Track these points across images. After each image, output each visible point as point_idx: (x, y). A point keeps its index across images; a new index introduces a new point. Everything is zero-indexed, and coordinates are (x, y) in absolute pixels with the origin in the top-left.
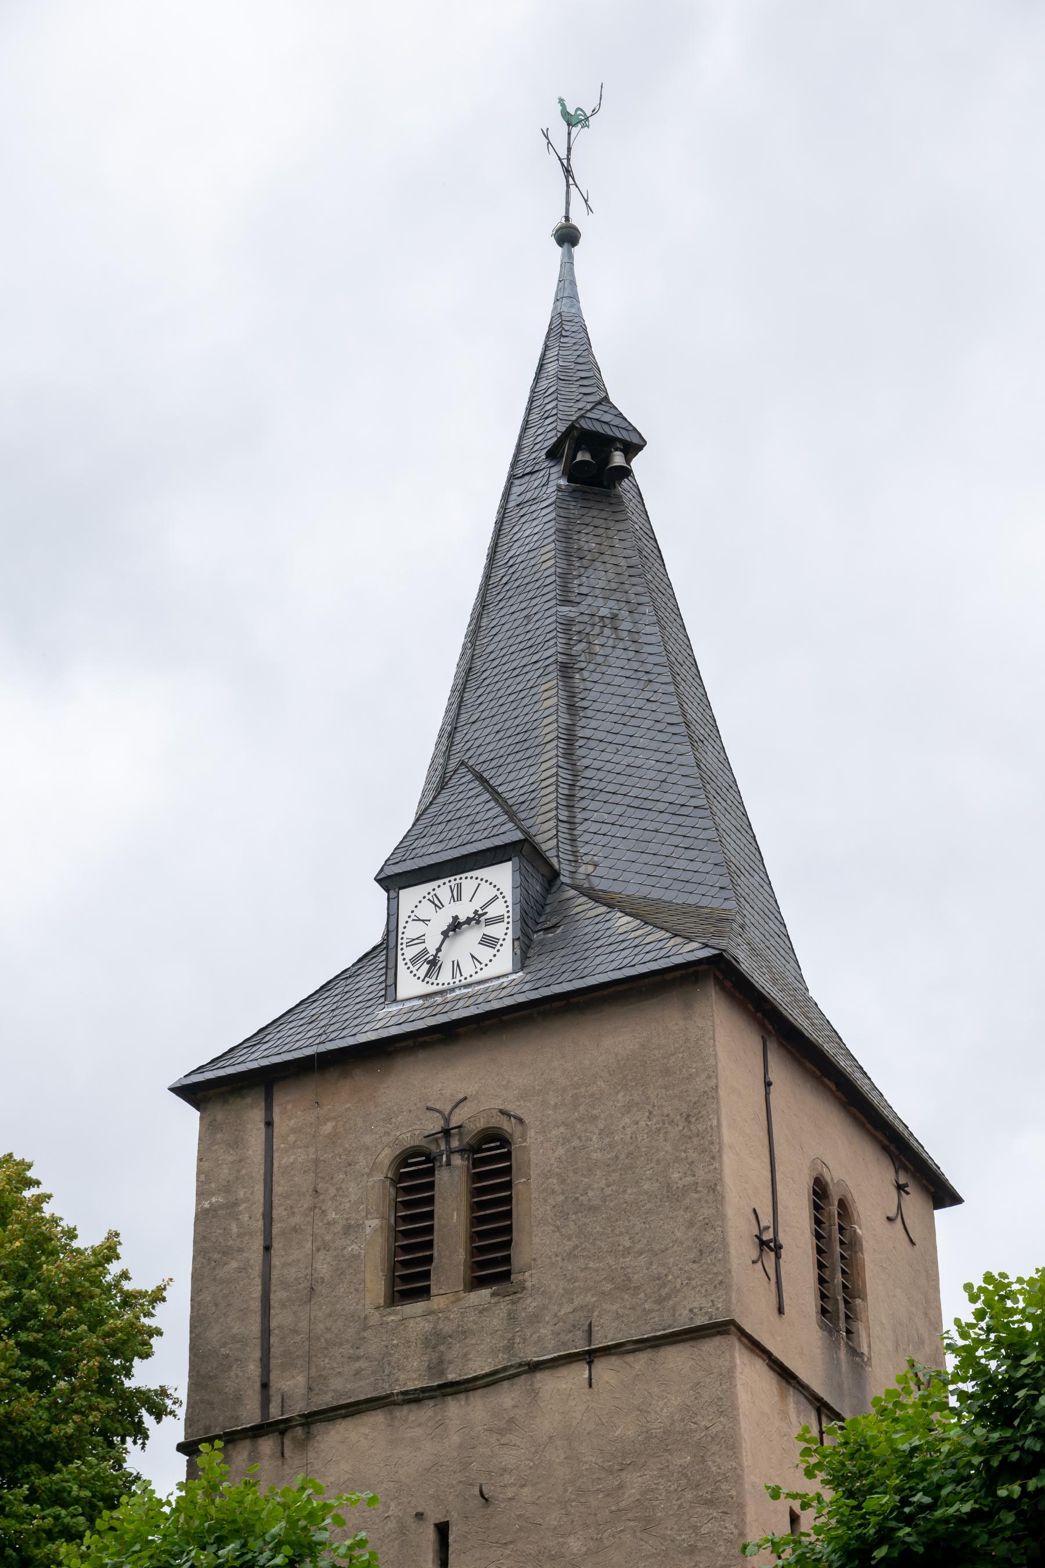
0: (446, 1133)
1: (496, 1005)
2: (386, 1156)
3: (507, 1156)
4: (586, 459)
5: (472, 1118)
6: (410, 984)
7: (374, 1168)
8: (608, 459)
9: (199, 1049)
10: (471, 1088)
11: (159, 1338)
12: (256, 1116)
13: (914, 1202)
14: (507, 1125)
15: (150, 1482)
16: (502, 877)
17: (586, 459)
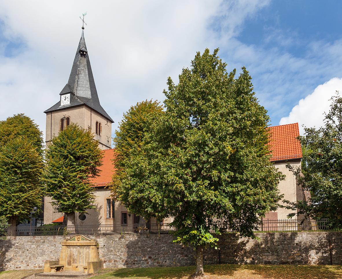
0: (64, 117)
1: (68, 107)
2: (60, 119)
3: (69, 120)
4: (82, 53)
5: (66, 116)
6: (62, 104)
7: (59, 120)
8: (84, 53)
9: (46, 109)
10: (66, 114)
11: (286, 177)
12: (51, 113)
13: (109, 123)
14: (69, 117)
15: (19, 114)
16: (69, 95)
17: (82, 53)
